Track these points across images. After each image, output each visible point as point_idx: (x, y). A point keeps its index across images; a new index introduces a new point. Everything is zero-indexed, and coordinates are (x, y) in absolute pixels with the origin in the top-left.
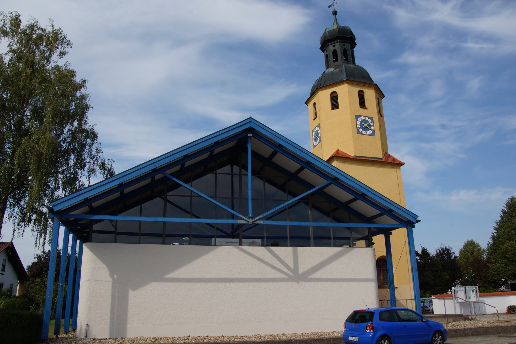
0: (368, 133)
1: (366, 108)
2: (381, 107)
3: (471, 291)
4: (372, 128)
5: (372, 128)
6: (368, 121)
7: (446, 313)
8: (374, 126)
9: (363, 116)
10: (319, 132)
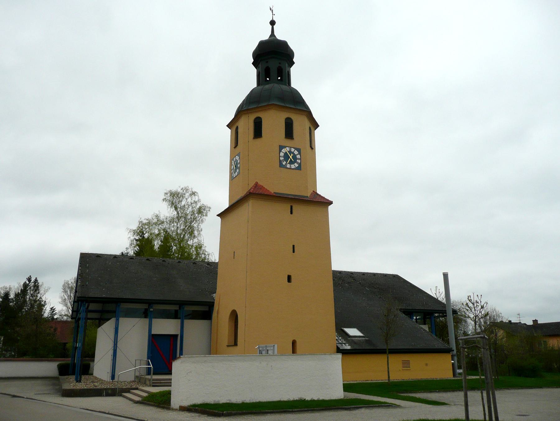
0: (293, 166)
2: (313, 138)
4: (299, 161)
5: (299, 161)
7: (466, 396)
8: (300, 159)
9: (289, 147)
10: (239, 162)
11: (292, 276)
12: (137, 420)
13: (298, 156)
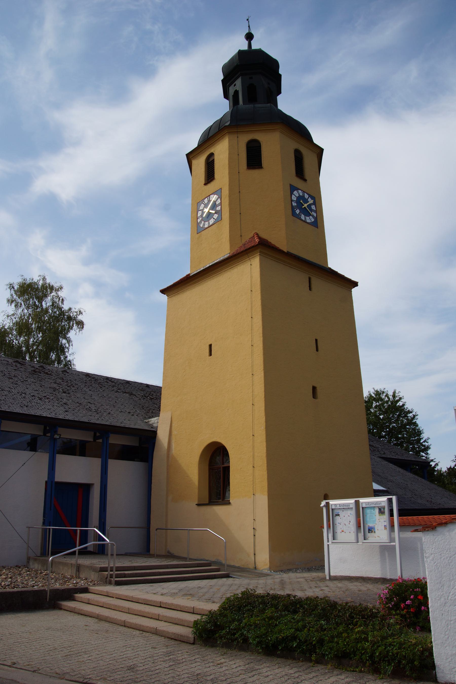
0: (309, 219)
1: (305, 180)
3: (377, 510)
6: (308, 200)
11: (318, 388)
12: (61, 676)
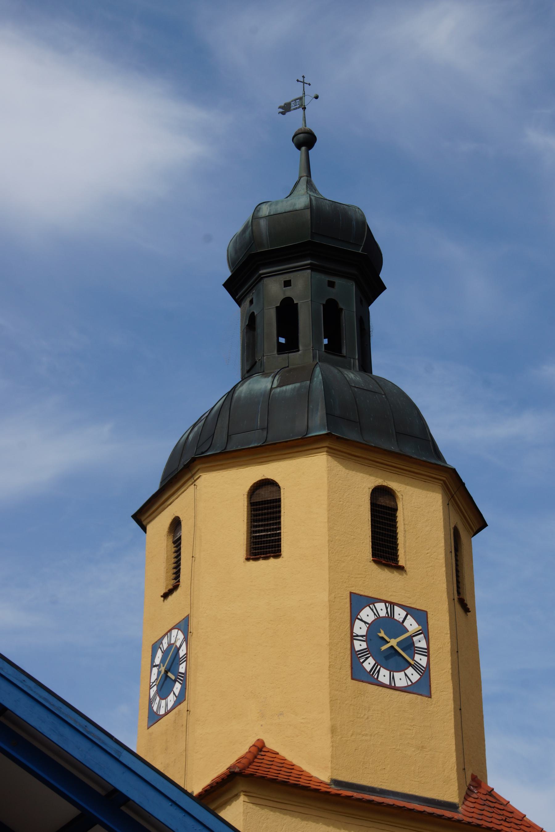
0: (400, 680)
4: (422, 660)
5: (422, 660)
10: (182, 653)
13: (420, 642)
